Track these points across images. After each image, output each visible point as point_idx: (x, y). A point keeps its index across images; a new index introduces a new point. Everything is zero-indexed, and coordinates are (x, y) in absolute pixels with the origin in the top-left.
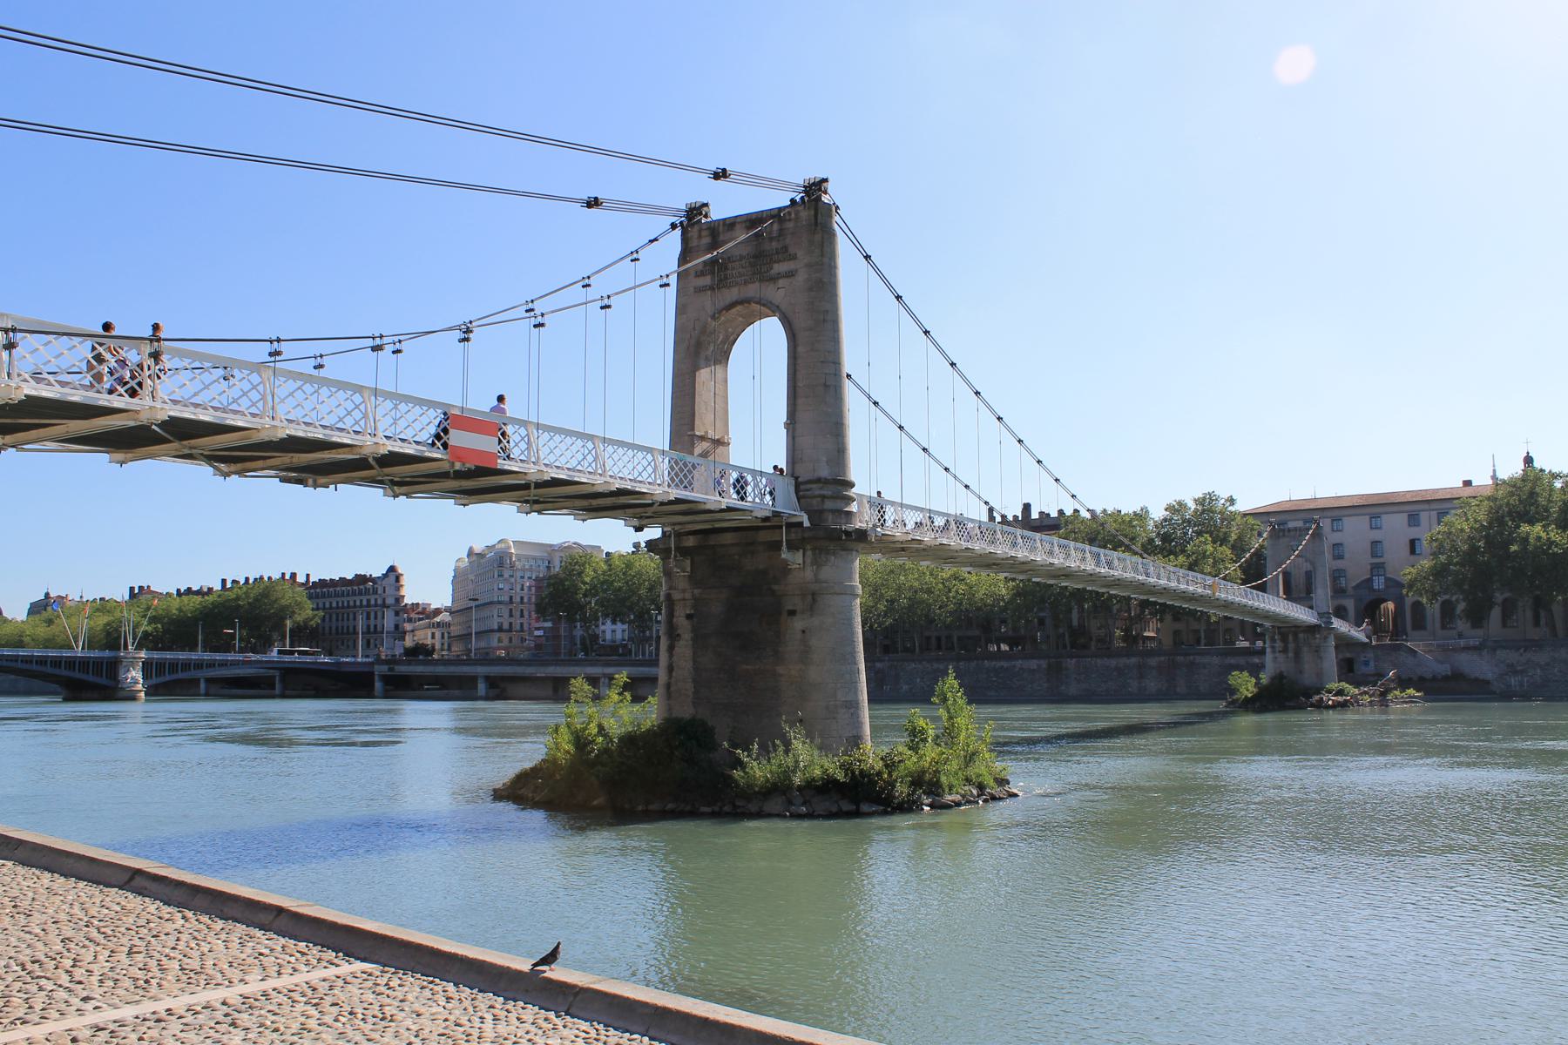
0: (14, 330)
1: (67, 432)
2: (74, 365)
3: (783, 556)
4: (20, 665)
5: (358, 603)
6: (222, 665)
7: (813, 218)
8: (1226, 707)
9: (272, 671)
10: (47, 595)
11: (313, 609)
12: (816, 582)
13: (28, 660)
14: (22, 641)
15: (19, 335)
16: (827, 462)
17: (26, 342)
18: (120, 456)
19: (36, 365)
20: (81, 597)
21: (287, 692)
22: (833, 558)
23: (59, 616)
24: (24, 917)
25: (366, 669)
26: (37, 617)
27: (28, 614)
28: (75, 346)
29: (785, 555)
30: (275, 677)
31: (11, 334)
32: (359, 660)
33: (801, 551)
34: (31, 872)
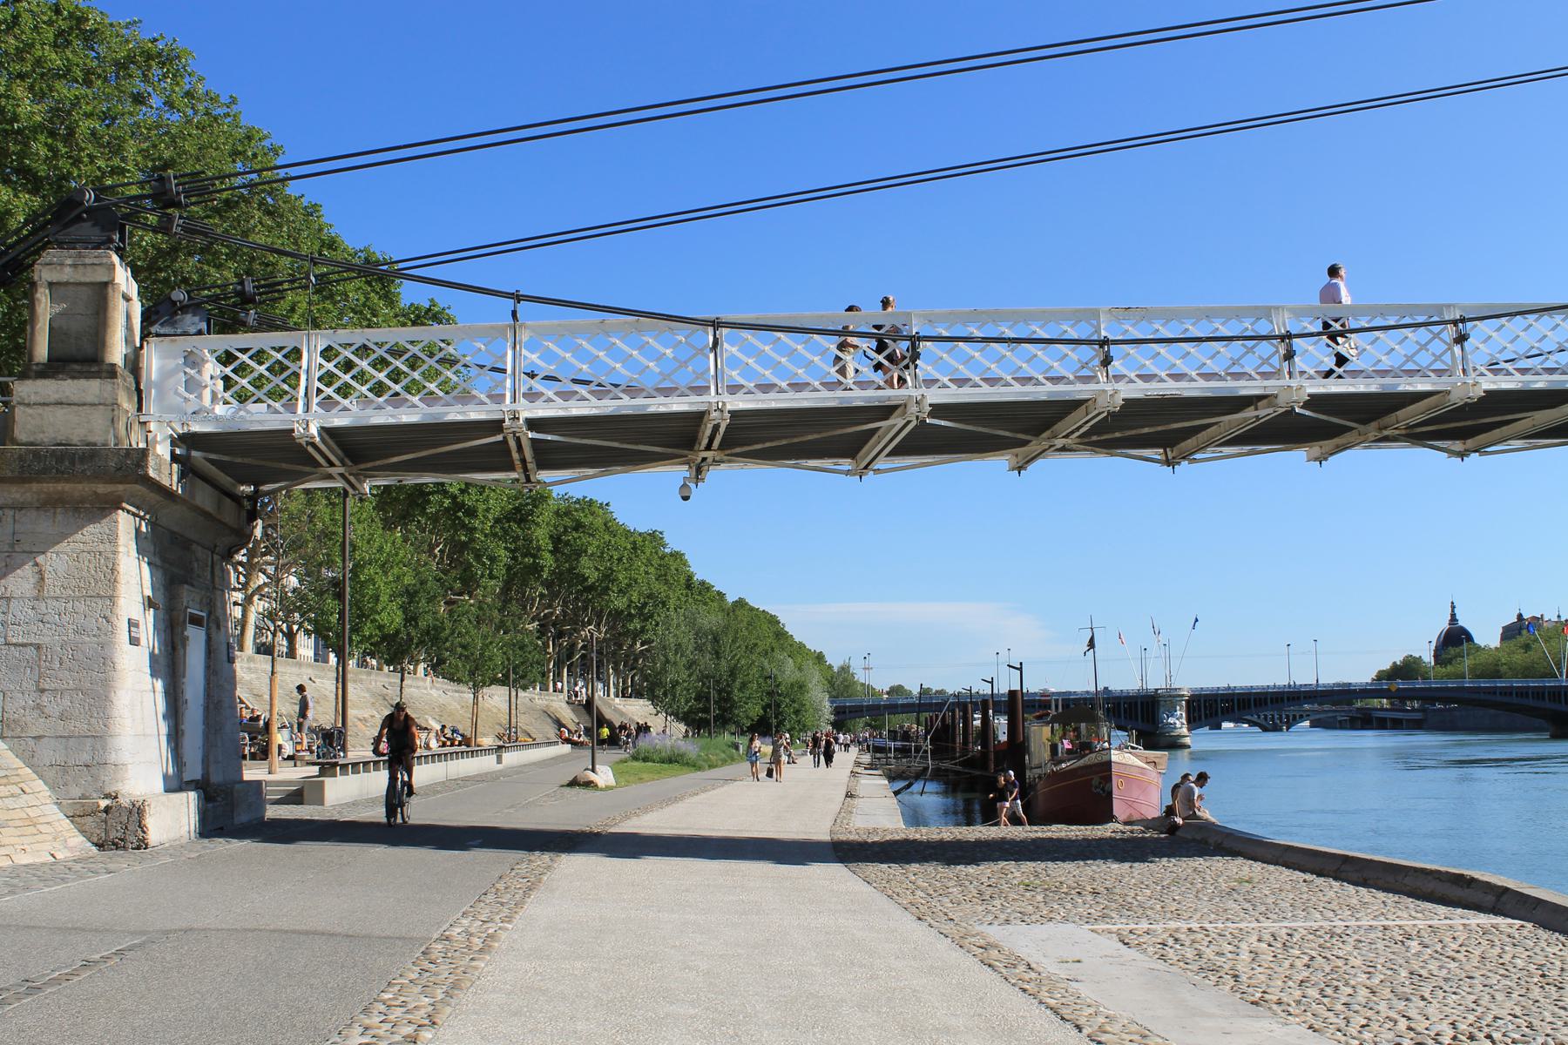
0: (1463, 320)
1: (1534, 426)
2: (1533, 347)
4: (1499, 698)
6: (1293, 698)
8: (1092, 779)
10: (1520, 616)
13: (1507, 692)
14: (1498, 671)
15: (1469, 325)
17: (1477, 331)
18: (1316, 449)
19: (1491, 355)
20: (1559, 616)
23: (1536, 640)
24: (1555, 989)
26: (1512, 643)
27: (1502, 639)
28: (1531, 325)
31: (1460, 325)
34: (1554, 937)
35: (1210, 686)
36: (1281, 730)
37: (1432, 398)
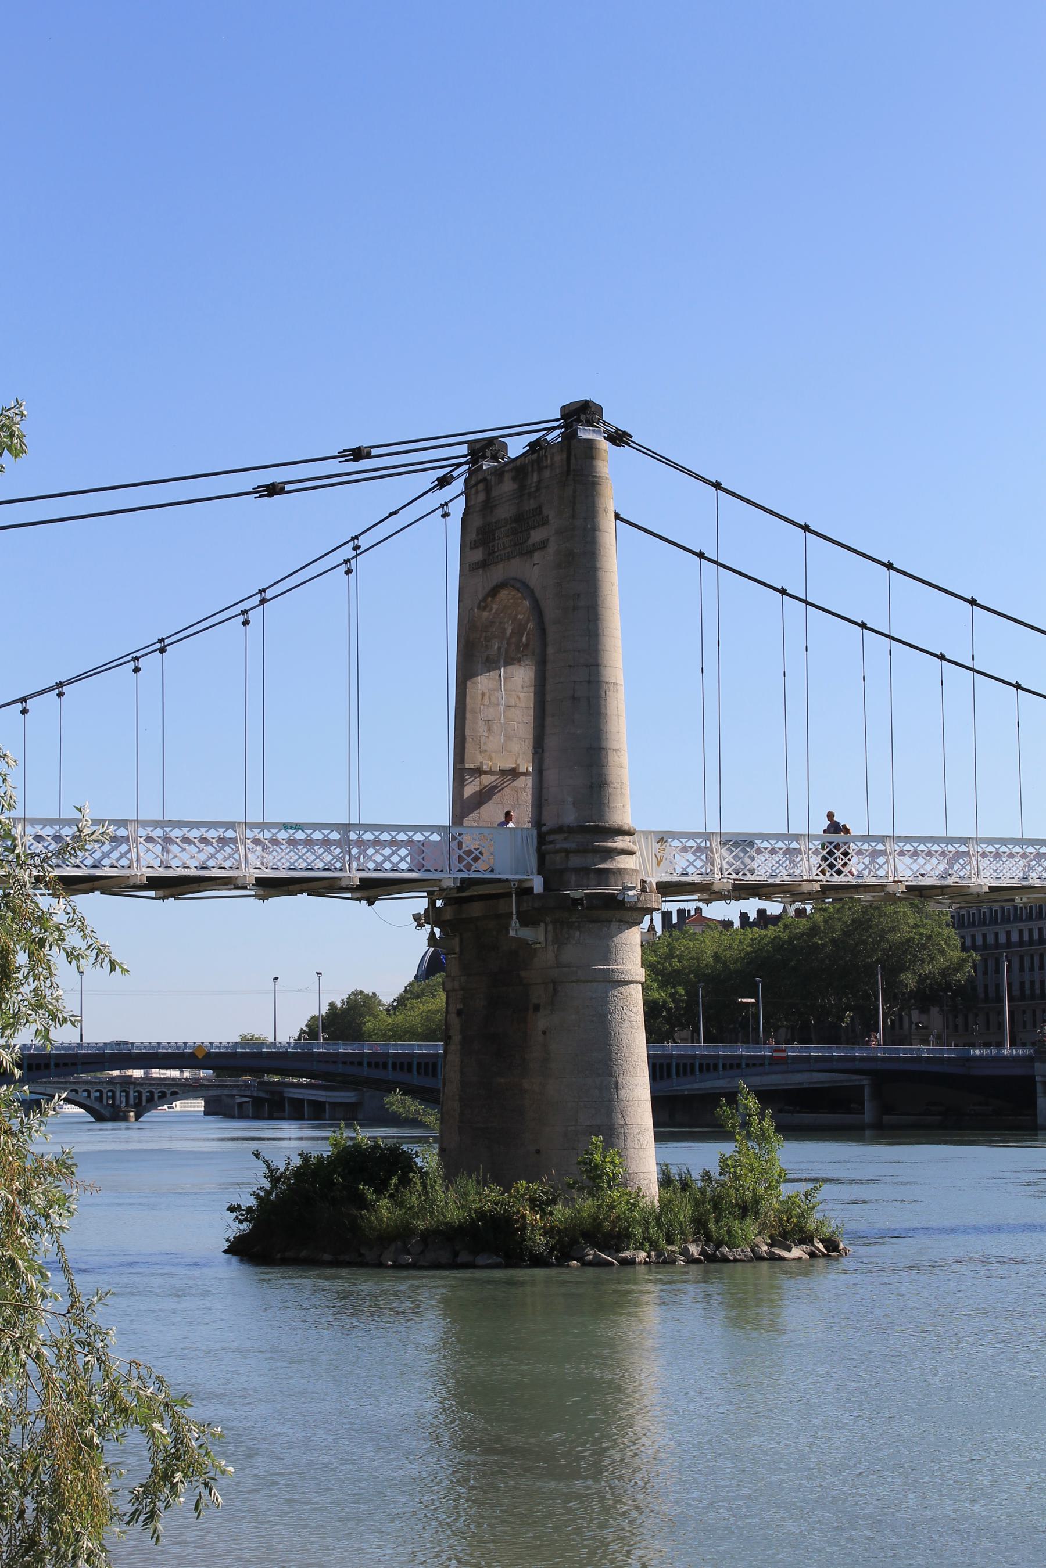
3: (512, 933)
5: (1002, 939)
6: (731, 1066)
7: (565, 463)
9: (855, 1077)
11: (964, 949)
12: (558, 967)
16: (574, 804)
21: (275, 1114)
22: (578, 933)
25: (1019, 1071)
29: (516, 931)
30: (861, 1088)
32: (1007, 1052)
33: (542, 924)
35: (173, 1040)
36: (125, 1119)
37: (103, 881)
